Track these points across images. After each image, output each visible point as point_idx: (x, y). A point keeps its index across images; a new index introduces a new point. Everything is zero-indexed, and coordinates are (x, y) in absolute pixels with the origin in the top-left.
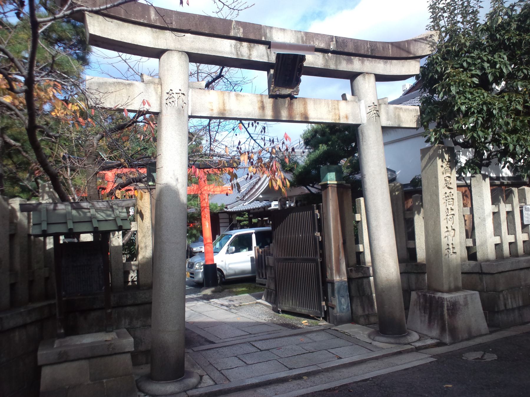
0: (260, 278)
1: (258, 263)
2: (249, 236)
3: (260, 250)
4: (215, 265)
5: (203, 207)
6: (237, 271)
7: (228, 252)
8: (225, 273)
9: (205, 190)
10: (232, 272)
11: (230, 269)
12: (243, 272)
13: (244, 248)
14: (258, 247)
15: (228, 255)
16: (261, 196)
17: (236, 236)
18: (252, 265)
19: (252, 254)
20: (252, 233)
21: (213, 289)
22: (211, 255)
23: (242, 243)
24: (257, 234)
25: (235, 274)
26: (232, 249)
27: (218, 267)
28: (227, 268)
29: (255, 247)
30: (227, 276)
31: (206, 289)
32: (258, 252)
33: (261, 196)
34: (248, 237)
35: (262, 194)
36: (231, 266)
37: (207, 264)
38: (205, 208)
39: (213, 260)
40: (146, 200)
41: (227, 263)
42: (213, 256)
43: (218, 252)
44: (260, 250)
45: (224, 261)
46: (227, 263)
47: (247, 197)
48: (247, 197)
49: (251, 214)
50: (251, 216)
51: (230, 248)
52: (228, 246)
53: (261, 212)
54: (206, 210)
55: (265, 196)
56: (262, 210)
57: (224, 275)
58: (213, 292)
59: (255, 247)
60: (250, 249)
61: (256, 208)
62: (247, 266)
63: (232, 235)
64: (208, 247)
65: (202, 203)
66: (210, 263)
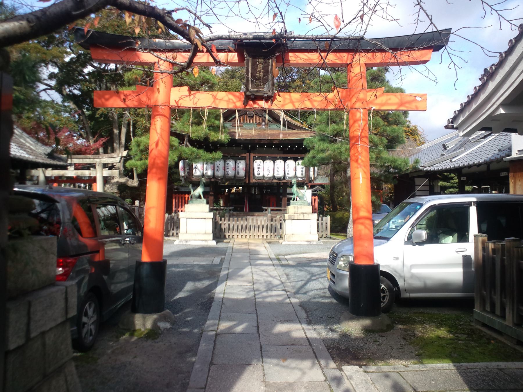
0: (484, 310)
1: (479, 271)
2: (464, 208)
3: (491, 246)
4: (377, 266)
5: (354, 137)
6: (429, 283)
7: (410, 240)
8: (401, 283)
9: (358, 100)
10: (417, 284)
11: (413, 276)
12: (445, 287)
13: (449, 232)
14: (485, 237)
15: (411, 246)
16: (502, 111)
17: (432, 208)
18: (465, 273)
19: (469, 248)
20: (470, 204)
21: (367, 322)
22: (366, 244)
23: (446, 224)
24: (480, 206)
25: (425, 289)
26: (420, 236)
27: (381, 269)
28: (407, 275)
29: (475, 236)
30: (406, 291)
31: (351, 319)
32: (484, 249)
33: (502, 111)
34: (462, 210)
35: (503, 105)
36: (414, 271)
37: (357, 263)
38: (357, 141)
39: (372, 257)
40: (268, 132)
41: (408, 263)
42: (372, 245)
43: (388, 239)
44: (491, 246)
45: (401, 259)
46: (408, 263)
47: (461, 119)
48: (461, 119)
49: (464, 175)
50: (464, 179)
51: (417, 231)
52: (413, 226)
53: (481, 173)
54: (359, 144)
55: (513, 111)
56: (484, 168)
57: (399, 288)
58: (367, 330)
59: (475, 236)
60: (463, 237)
61: (474, 165)
62: (455, 274)
63: (421, 205)
64: (361, 227)
65: (352, 129)
66: (364, 262)
